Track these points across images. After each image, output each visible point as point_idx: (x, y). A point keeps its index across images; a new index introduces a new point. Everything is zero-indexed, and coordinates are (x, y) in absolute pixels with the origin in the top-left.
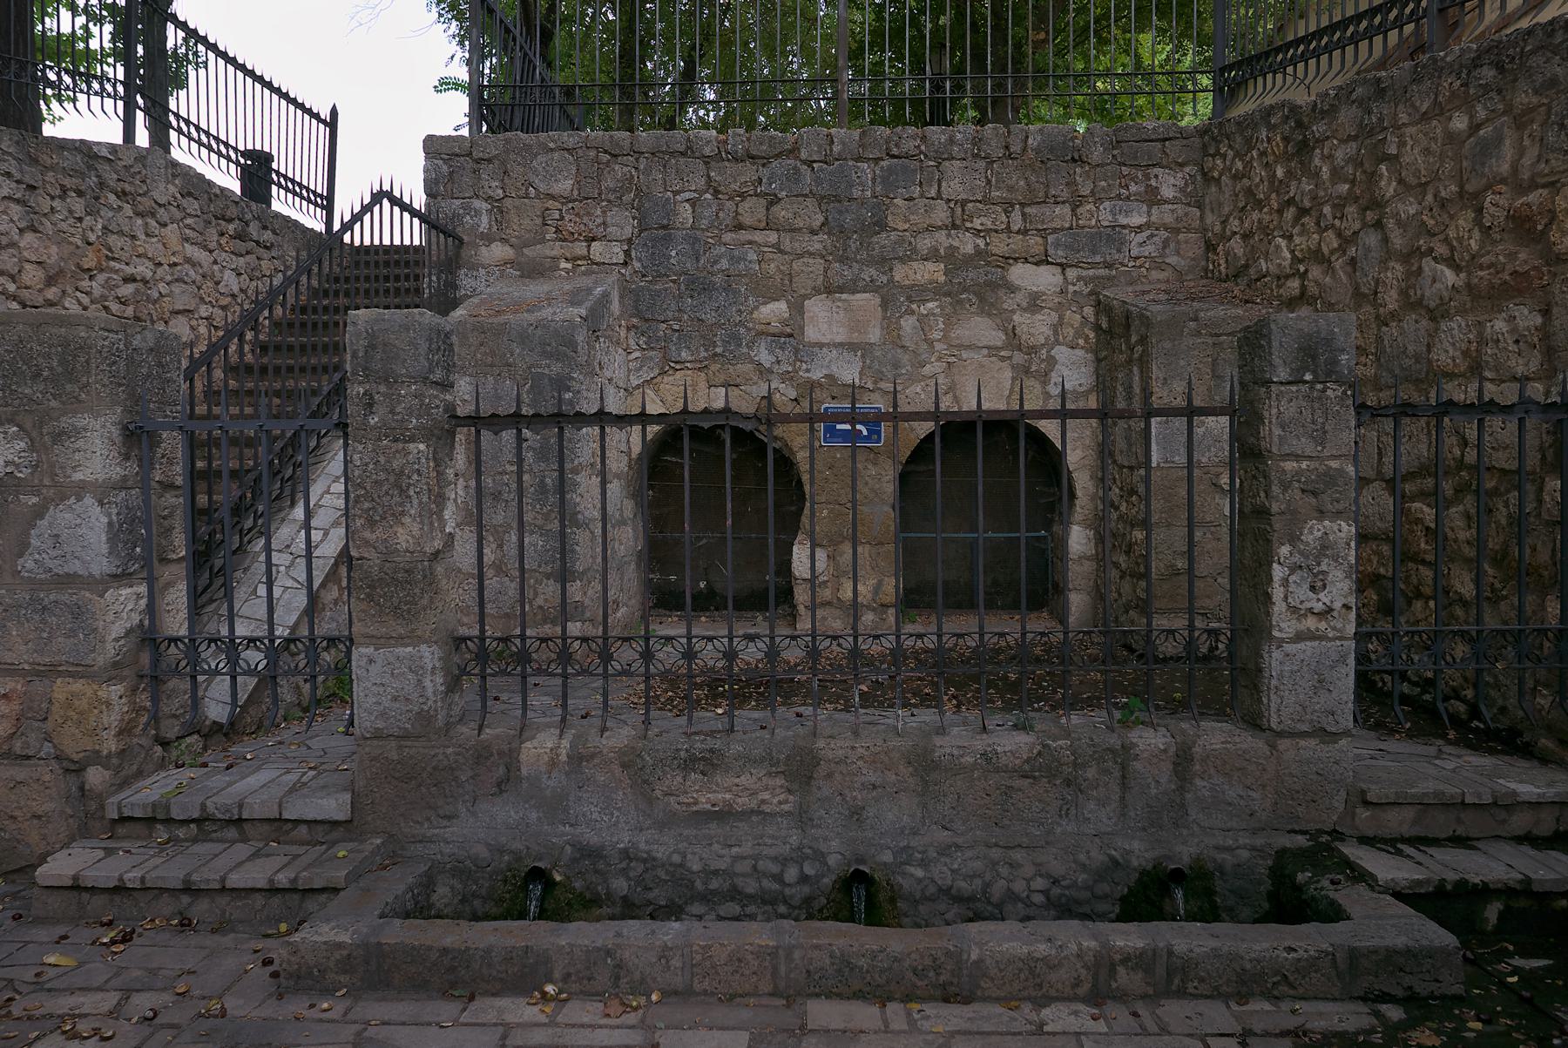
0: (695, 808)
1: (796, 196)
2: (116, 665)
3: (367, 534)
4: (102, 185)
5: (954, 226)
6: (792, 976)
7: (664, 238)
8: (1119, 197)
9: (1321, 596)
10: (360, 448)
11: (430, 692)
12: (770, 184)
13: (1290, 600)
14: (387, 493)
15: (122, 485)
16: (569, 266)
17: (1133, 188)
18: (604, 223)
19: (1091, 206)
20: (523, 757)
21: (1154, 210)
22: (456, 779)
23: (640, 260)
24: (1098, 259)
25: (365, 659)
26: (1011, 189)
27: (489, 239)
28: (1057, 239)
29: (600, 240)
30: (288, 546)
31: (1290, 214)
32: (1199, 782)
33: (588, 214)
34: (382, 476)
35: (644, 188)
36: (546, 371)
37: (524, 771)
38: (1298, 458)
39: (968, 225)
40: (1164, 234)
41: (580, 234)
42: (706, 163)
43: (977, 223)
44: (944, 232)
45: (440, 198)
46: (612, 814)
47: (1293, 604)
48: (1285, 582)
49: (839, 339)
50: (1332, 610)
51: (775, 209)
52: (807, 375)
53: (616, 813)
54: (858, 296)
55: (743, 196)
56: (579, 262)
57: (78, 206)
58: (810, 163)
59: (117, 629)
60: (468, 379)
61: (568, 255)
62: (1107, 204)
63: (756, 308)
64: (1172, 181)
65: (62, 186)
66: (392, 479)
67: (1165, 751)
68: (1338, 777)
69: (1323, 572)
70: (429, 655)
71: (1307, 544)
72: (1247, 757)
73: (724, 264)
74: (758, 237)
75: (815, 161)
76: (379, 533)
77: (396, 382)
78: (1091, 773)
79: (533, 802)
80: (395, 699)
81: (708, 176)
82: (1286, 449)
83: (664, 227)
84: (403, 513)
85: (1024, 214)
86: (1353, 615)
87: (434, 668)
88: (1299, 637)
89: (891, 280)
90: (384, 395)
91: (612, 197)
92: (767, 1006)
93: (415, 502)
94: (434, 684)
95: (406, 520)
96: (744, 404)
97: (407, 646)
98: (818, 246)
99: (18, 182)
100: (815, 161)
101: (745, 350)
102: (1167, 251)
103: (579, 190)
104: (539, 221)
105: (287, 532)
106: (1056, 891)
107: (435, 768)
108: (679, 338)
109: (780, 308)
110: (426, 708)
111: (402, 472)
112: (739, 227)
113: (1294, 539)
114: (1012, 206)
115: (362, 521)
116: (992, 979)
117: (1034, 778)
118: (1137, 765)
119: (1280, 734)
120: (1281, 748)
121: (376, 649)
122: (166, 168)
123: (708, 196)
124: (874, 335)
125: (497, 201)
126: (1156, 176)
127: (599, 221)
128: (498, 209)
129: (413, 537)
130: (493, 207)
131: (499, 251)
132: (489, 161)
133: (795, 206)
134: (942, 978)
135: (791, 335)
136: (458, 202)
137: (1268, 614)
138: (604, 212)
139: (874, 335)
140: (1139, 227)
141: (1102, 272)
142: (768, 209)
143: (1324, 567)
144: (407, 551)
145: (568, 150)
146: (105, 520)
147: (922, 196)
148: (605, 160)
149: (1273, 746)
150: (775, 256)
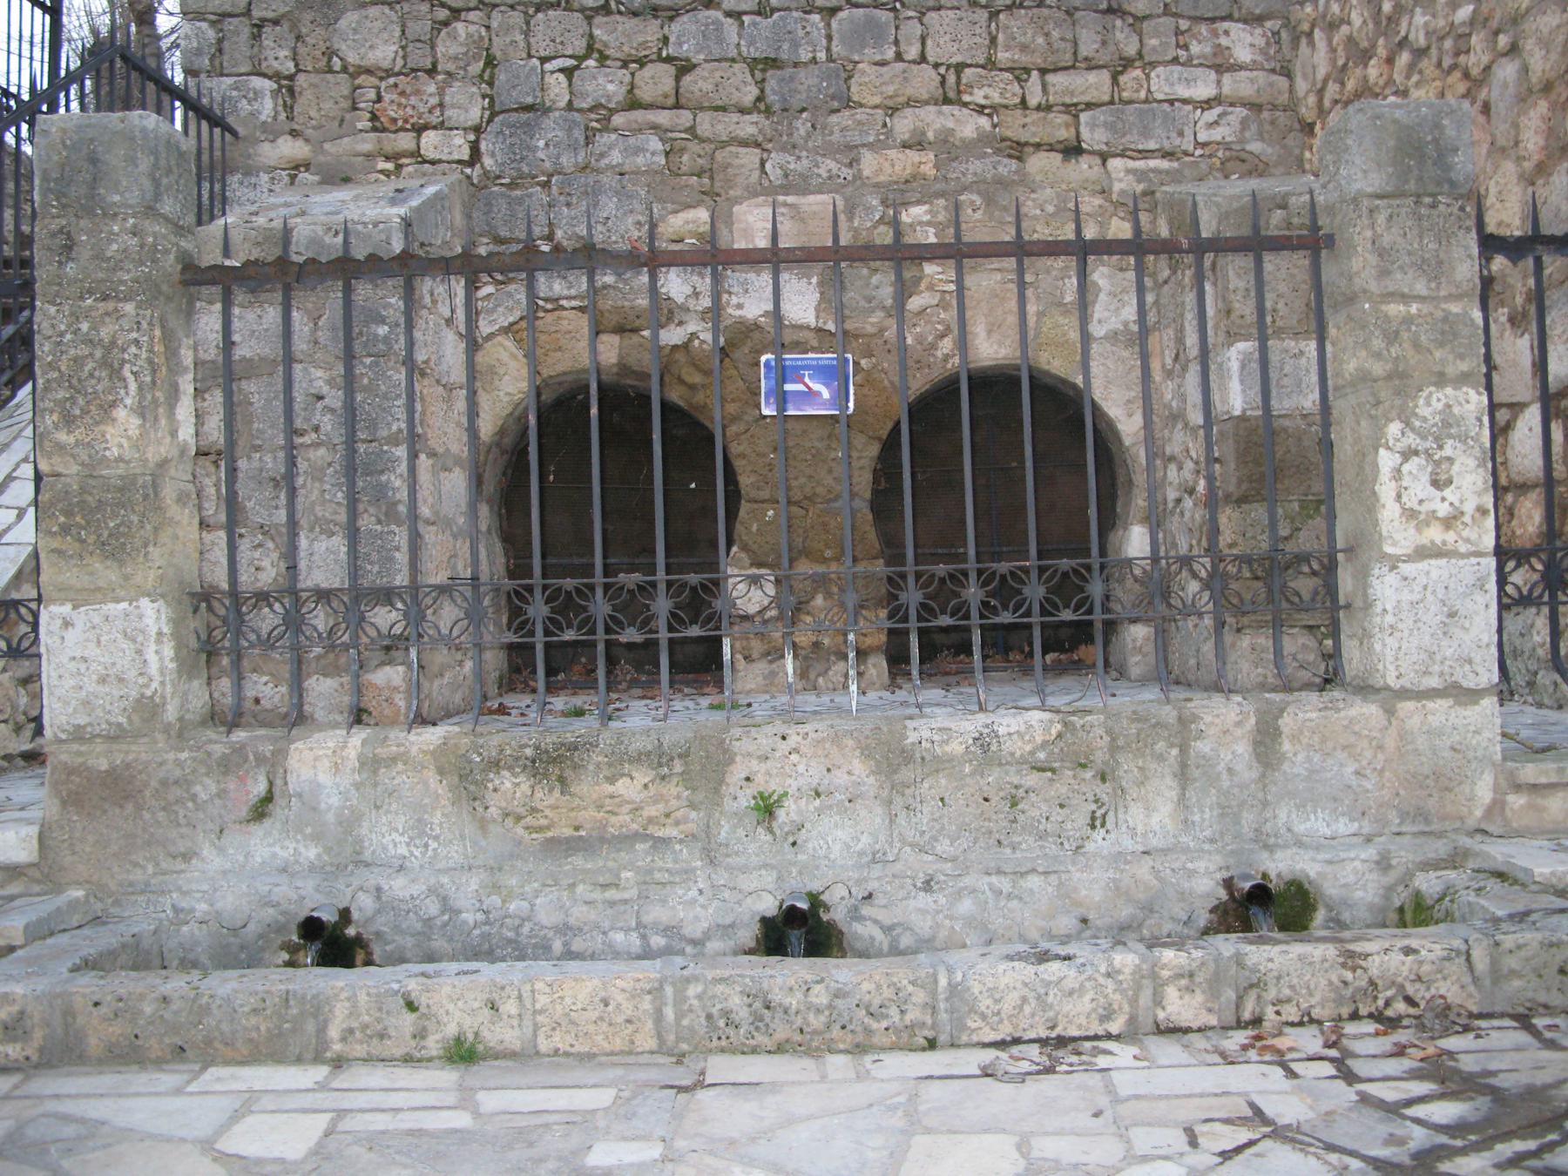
0: (550, 834)
3: (62, 437)
5: (947, 101)
6: (685, 1022)
7: (527, 124)
8: (1175, 61)
9: (1447, 493)
10: (53, 310)
11: (153, 668)
12: (680, 45)
13: (1404, 499)
14: (91, 375)
17: (1195, 48)
18: (441, 105)
19: (1138, 73)
21: (1227, 79)
22: (194, 798)
23: (493, 155)
24: (1152, 145)
25: (59, 622)
26: (1024, 48)
27: (271, 133)
28: (1093, 118)
29: (435, 128)
31: (1404, 58)
33: (417, 92)
34: (84, 350)
38: (1405, 298)
39: (966, 98)
40: (1241, 112)
41: (406, 121)
42: (589, 19)
43: (978, 96)
44: (932, 108)
46: (426, 846)
48: (1397, 474)
50: (1462, 513)
51: (687, 79)
52: (738, 313)
53: (433, 845)
54: (811, 198)
55: (642, 62)
62: (1160, 69)
64: (1249, 39)
66: (98, 353)
69: (1450, 460)
70: (153, 616)
71: (1425, 419)
72: (1357, 728)
73: (616, 157)
74: (663, 118)
75: (746, 13)
76: (79, 433)
77: (105, 215)
79: (309, 830)
80: (103, 680)
81: (591, 36)
84: (113, 405)
85: (1044, 86)
86: (1490, 522)
87: (160, 634)
88: (1423, 553)
89: (858, 176)
90: (89, 233)
91: (451, 67)
92: (648, 1064)
93: (133, 386)
94: (160, 658)
97: (117, 600)
98: (752, 130)
100: (746, 13)
102: (1247, 134)
103: (404, 57)
104: (346, 104)
110: (149, 693)
111: (113, 343)
114: (1027, 71)
115: (55, 417)
116: (984, 1017)
117: (1053, 771)
119: (1404, 694)
121: (75, 608)
123: (591, 63)
126: (1227, 33)
127: (434, 101)
128: (287, 87)
129: (129, 438)
130: (280, 87)
132: (276, 22)
134: (908, 1018)
136: (229, 81)
137: (1376, 524)
140: (1208, 102)
141: (1164, 164)
143: (1448, 451)
144: (120, 459)
147: (899, 57)
149: (1390, 712)
150: (689, 144)
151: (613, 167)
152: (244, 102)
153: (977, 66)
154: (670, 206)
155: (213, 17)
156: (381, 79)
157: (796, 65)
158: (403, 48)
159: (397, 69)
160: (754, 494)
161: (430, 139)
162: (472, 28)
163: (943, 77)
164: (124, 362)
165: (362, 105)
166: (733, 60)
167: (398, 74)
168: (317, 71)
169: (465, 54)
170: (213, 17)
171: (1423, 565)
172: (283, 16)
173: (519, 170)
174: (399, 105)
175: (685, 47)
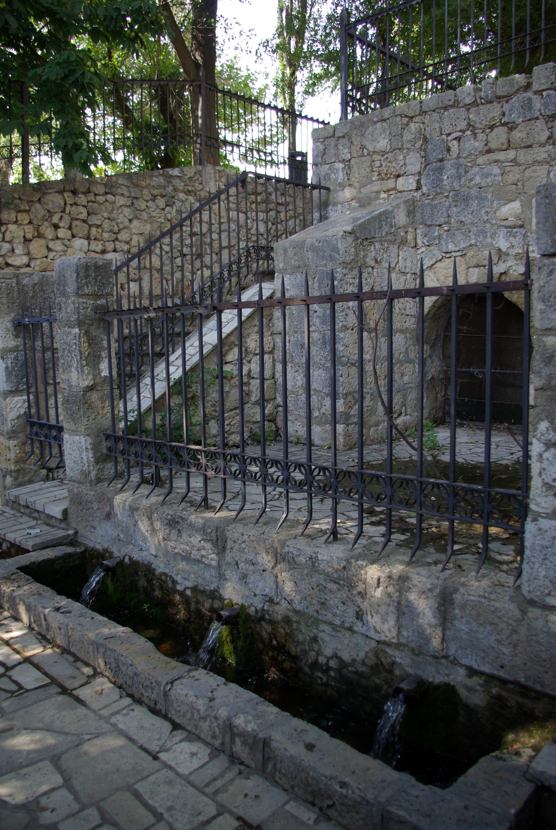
1: (529, 120)
2: (13, 432)
4: (175, 190)
12: (511, 115)
15: (15, 349)
27: (342, 186)
29: (403, 175)
36: (324, 269)
41: (391, 174)
47: (546, 480)
55: (492, 128)
56: (391, 193)
57: (161, 202)
58: (539, 93)
59: (12, 415)
63: (498, 208)
65: (152, 195)
73: (478, 180)
74: (501, 156)
75: (544, 90)
98: (545, 156)
99: (128, 197)
101: (489, 240)
103: (390, 145)
105: (161, 369)
108: (447, 236)
112: (489, 151)
122: (215, 173)
133: (528, 128)
146: (4, 366)
149: (524, 612)
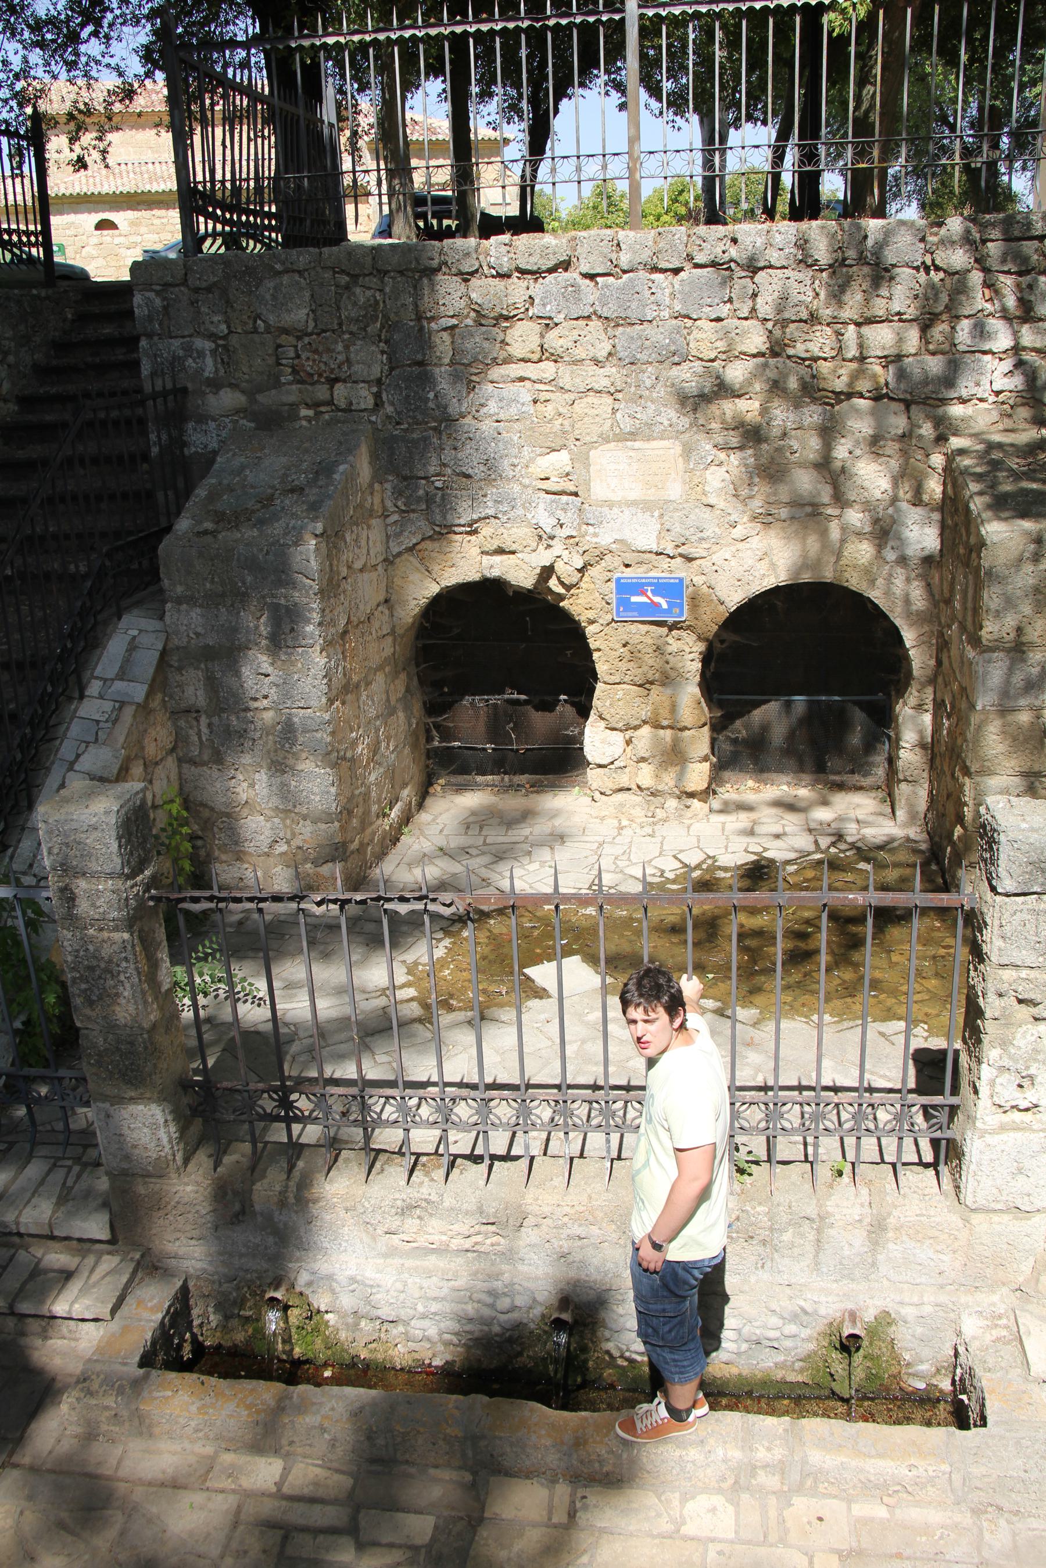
12: (544, 305)
16: (310, 413)
18: (348, 360)
20: (255, 1197)
23: (392, 404)
27: (215, 385)
29: (345, 381)
30: (31, 866)
32: (891, 1246)
33: (329, 350)
35: (392, 316)
37: (257, 1207)
41: (320, 375)
45: (156, 338)
49: (633, 496)
52: (595, 540)
54: (655, 444)
56: (323, 409)
60: (198, 610)
61: (309, 401)
67: (860, 1221)
68: (1027, 1247)
71: (1019, 1048)
74: (529, 370)
78: (787, 1237)
82: (1005, 961)
83: (421, 364)
87: (166, 1121)
88: (1003, 1128)
91: (354, 328)
93: (128, 985)
95: (123, 1001)
96: (522, 574)
98: (605, 382)
103: (315, 320)
104: (271, 361)
106: (746, 1330)
107: (178, 1203)
109: (563, 458)
113: (1004, 1044)
118: (832, 1232)
120: (973, 1222)
124: (675, 490)
125: (221, 338)
127: (341, 358)
128: (225, 353)
130: (218, 346)
131: (229, 399)
135: (576, 494)
138: (347, 347)
139: (675, 490)
142: (542, 336)
145: (299, 272)
148: (343, 283)
151: (491, 416)
152: (190, 360)
153: (801, 321)
154: (538, 450)
155: (158, 288)
156: (299, 338)
157: (642, 322)
158: (313, 311)
159: (310, 330)
160: (607, 679)
161: (340, 390)
162: (369, 293)
163: (770, 332)
164: (119, 972)
165: (284, 362)
166: (588, 318)
167: (311, 334)
168: (246, 333)
169: (364, 316)
170: (158, 288)
171: (1004, 1136)
172: (215, 284)
173: (414, 418)
174: (314, 361)
175: (548, 308)
